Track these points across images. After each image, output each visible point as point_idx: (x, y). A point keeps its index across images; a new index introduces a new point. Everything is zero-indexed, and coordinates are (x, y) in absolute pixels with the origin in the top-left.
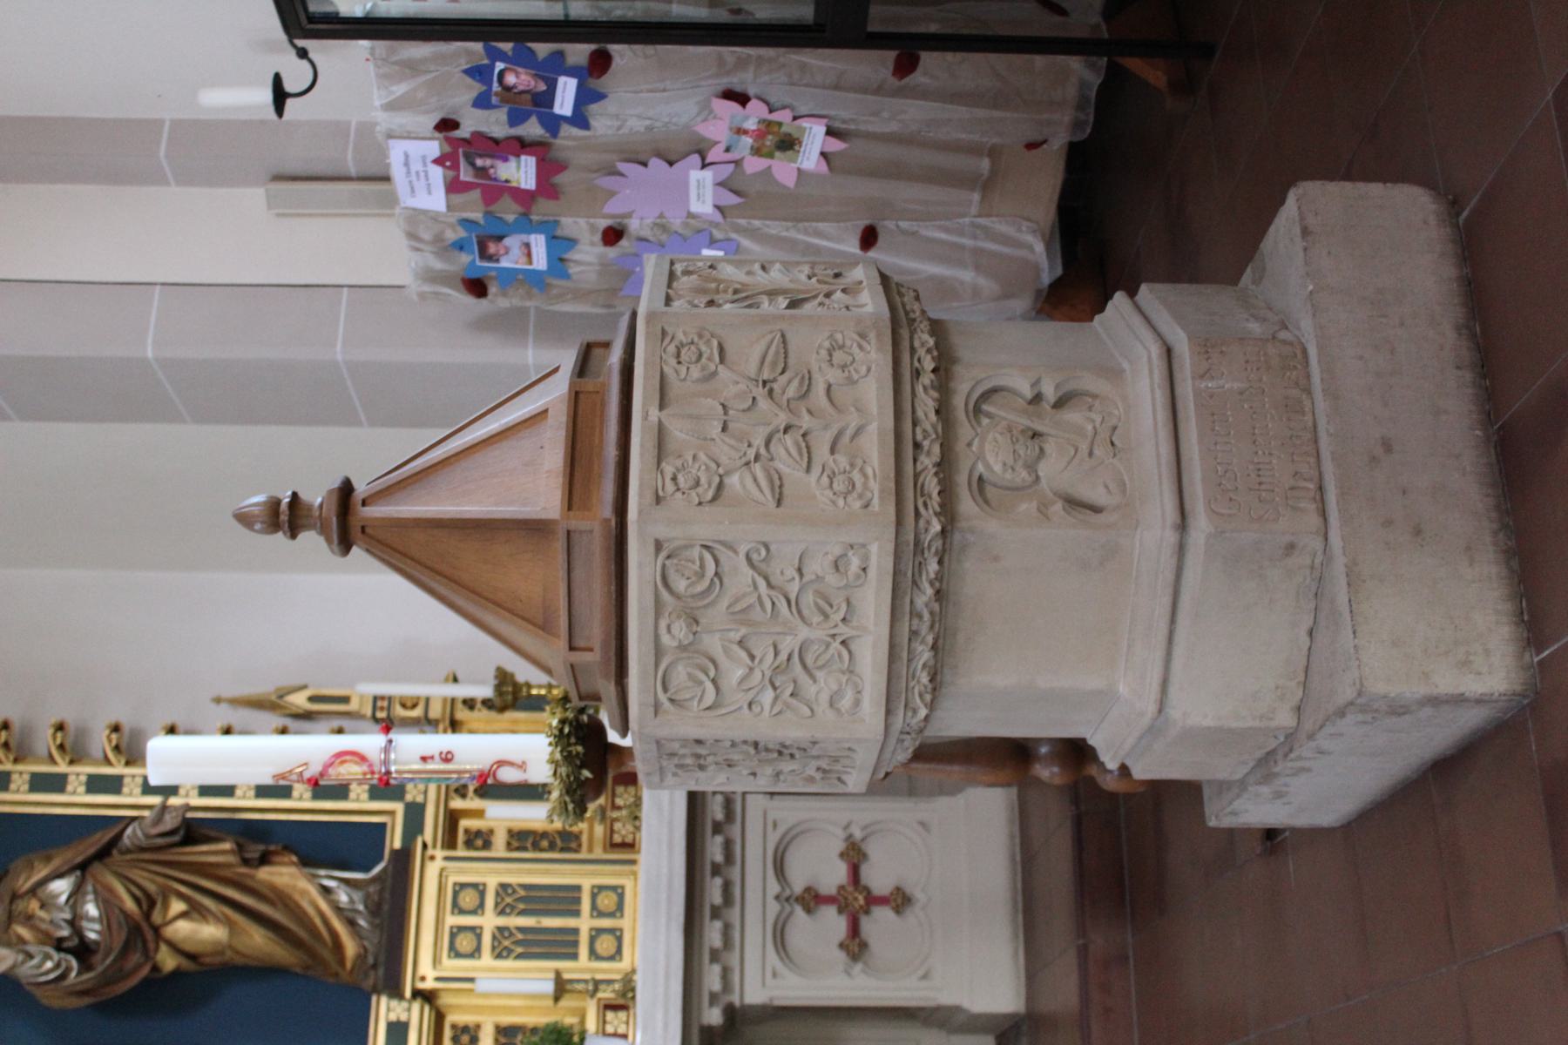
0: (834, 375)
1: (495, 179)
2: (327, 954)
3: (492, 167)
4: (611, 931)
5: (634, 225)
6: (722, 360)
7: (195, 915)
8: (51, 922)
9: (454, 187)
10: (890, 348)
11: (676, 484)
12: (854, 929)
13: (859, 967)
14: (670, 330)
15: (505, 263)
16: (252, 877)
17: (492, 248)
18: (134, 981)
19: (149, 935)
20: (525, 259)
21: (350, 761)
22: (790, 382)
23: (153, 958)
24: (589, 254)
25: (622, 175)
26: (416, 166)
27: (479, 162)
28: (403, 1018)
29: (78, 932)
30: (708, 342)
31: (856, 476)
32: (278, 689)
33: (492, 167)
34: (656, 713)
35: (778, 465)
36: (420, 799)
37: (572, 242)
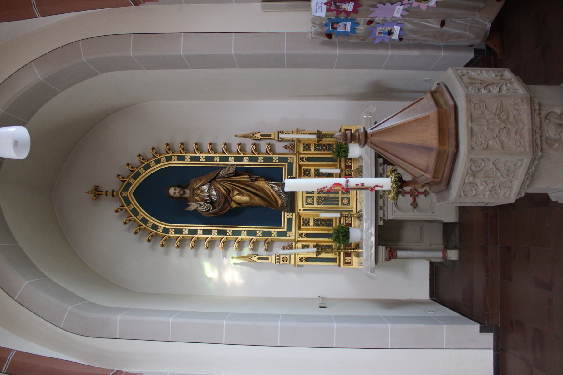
0: (515, 112)
1: (341, 9)
2: (274, 203)
3: (341, 5)
4: (347, 197)
5: (377, 20)
6: (486, 109)
7: (240, 194)
8: (204, 196)
9: (328, 10)
10: (530, 105)
11: (476, 144)
12: (414, 200)
13: (416, 210)
14: (472, 99)
15: (338, 30)
16: (253, 184)
17: (335, 26)
18: (225, 211)
19: (230, 199)
20: (344, 29)
21: (338, 186)
22: (504, 115)
23: (230, 205)
24: (361, 28)
25: (377, 7)
26: (319, 5)
27: (337, 4)
28: (291, 217)
29: (211, 198)
30: (482, 104)
31: (522, 141)
32: (252, 133)
33: (341, 5)
34: (460, 197)
35: (502, 138)
36: (292, 161)
37: (358, 24)
